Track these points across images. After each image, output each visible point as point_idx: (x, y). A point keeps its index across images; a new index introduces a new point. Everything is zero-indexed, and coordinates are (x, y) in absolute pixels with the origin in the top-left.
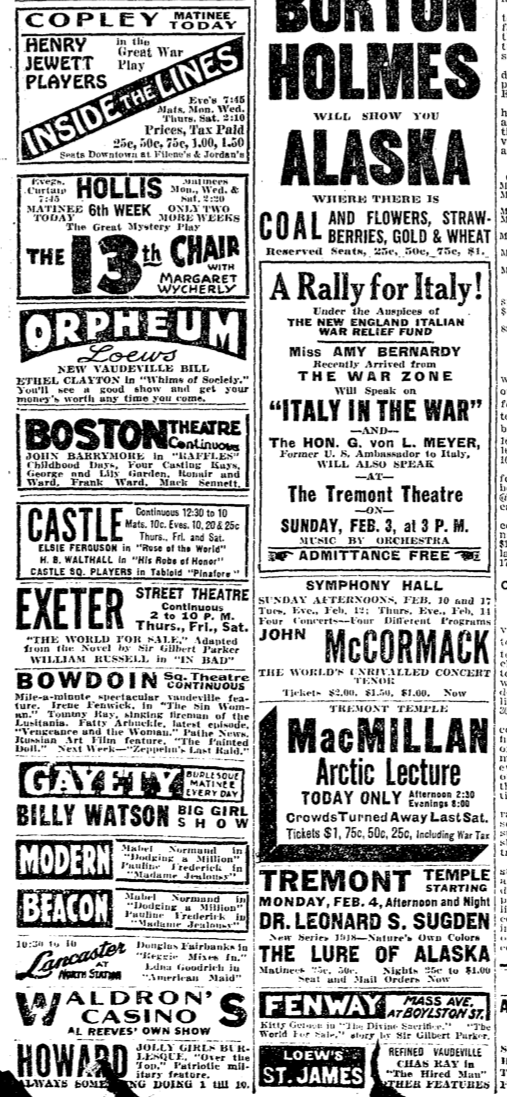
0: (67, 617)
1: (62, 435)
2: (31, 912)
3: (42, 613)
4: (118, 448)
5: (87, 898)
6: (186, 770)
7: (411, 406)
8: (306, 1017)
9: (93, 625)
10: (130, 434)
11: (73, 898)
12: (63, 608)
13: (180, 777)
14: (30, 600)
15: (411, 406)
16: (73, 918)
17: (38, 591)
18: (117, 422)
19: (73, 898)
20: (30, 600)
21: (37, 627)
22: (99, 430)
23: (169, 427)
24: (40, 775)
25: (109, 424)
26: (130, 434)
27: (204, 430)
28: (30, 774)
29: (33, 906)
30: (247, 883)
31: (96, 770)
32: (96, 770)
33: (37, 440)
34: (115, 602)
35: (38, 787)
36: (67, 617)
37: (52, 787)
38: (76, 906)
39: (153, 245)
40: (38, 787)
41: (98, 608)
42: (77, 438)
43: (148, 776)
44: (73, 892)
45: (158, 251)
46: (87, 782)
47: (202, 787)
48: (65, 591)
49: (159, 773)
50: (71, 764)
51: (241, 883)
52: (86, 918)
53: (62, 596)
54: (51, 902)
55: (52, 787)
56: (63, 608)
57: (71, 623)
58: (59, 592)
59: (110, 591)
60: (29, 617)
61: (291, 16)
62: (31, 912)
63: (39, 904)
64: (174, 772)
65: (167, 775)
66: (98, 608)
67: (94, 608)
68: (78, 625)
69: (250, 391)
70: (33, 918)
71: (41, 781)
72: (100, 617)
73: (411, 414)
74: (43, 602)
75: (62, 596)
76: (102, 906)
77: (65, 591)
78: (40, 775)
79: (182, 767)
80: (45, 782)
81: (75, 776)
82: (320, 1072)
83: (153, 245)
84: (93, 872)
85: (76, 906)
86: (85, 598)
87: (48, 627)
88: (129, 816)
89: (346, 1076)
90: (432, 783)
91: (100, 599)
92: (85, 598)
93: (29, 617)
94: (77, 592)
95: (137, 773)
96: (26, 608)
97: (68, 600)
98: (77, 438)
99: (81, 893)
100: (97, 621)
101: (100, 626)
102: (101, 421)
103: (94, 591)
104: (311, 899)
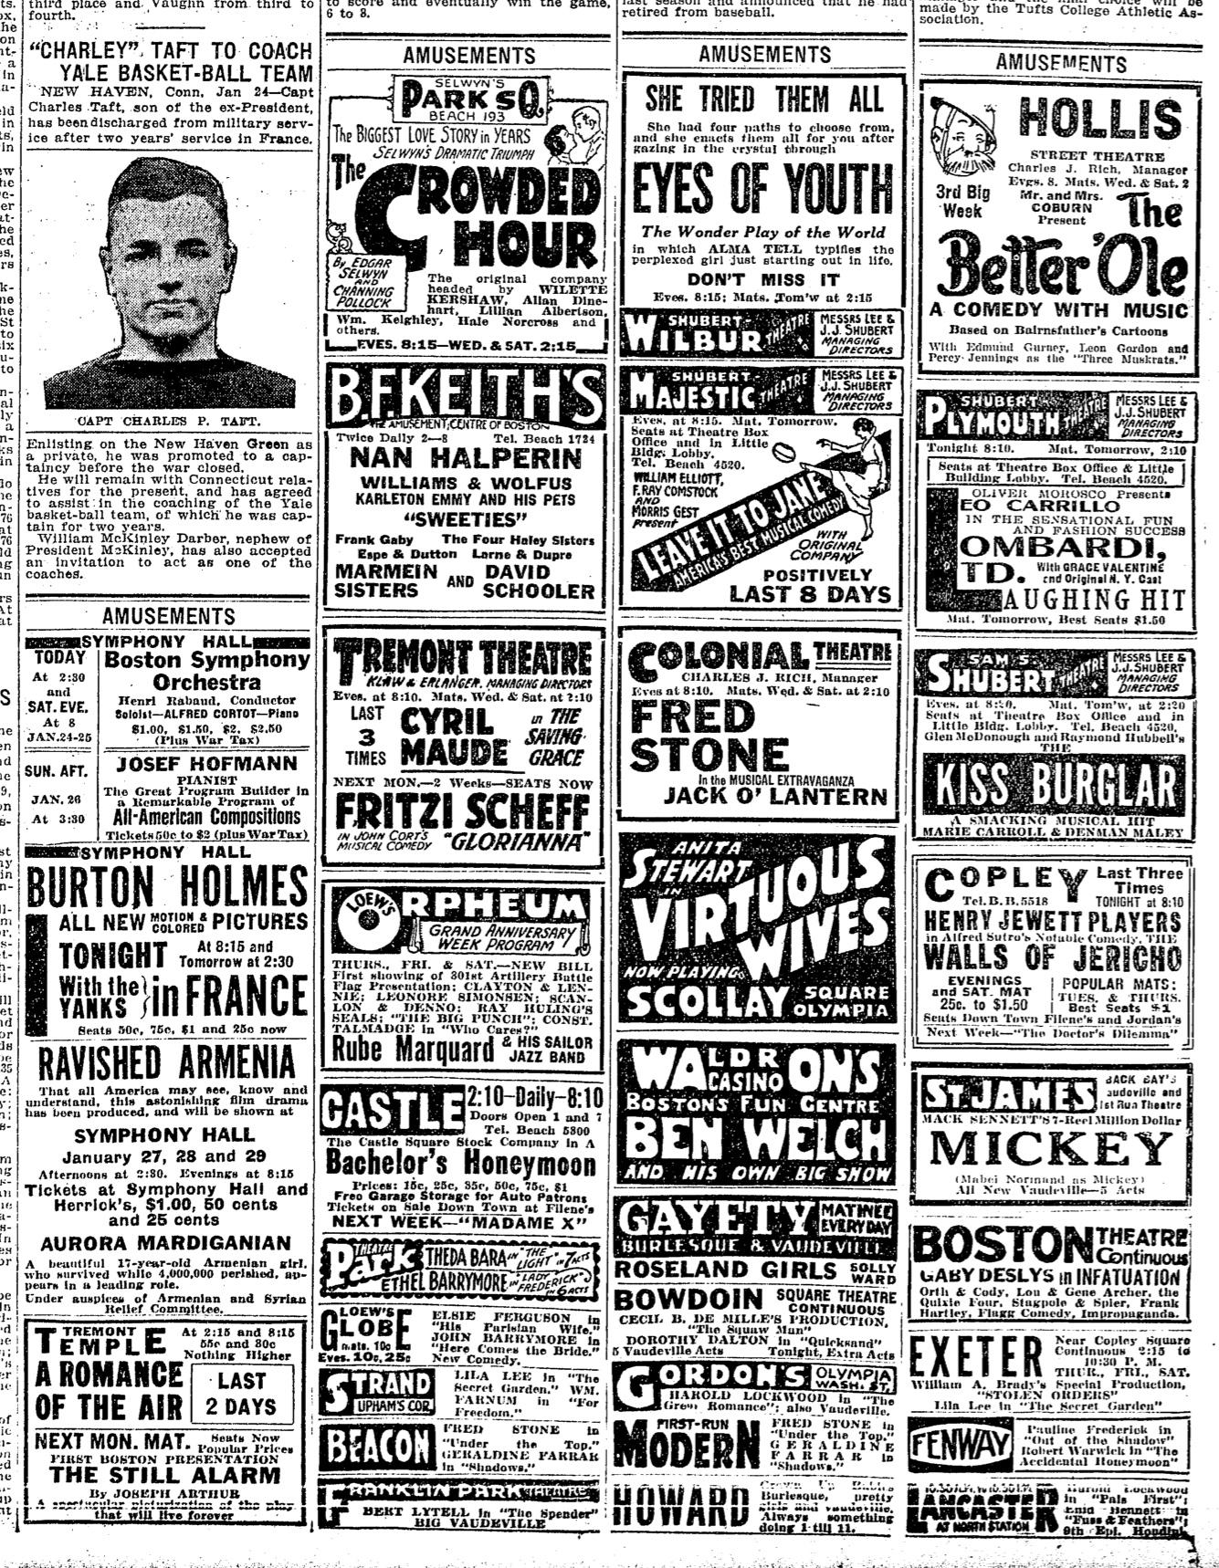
0: (973, 1364)
1: (958, 1244)
2: (337, 1452)
3: (940, 1361)
4: (1031, 1260)
5: (403, 1435)
8: (555, 367)
10: (1047, 1244)
11: (388, 1434)
13: (814, 1211)
16: (388, 1458)
18: (1028, 1229)
19: (388, 1434)
20: (926, 1349)
22: (1007, 1240)
23: (1097, 1235)
24: (636, 1211)
25: (1019, 1232)
26: (1047, 1244)
27: (1143, 1239)
29: (339, 1444)
30: (602, 867)
31: (706, 1204)
33: (927, 1250)
35: (634, 1226)
36: (973, 1364)
38: (391, 1443)
40: (634, 1226)
42: (976, 1247)
44: (388, 1426)
46: (697, 1218)
49: (791, 1207)
52: (404, 1458)
54: (362, 1439)
62: (337, 1452)
63: (347, 1443)
64: (808, 1205)
65: (800, 1210)
67: (1007, 1356)
70: (340, 1459)
76: (422, 1444)
81: (680, 1211)
82: (795, 492)
85: (391, 1443)
89: (801, 1138)
91: (1017, 1348)
94: (986, 1340)
95: (763, 1207)
97: (974, 1348)
98: (976, 1247)
99: (397, 1428)
102: (1009, 1229)
104: (244, 1402)
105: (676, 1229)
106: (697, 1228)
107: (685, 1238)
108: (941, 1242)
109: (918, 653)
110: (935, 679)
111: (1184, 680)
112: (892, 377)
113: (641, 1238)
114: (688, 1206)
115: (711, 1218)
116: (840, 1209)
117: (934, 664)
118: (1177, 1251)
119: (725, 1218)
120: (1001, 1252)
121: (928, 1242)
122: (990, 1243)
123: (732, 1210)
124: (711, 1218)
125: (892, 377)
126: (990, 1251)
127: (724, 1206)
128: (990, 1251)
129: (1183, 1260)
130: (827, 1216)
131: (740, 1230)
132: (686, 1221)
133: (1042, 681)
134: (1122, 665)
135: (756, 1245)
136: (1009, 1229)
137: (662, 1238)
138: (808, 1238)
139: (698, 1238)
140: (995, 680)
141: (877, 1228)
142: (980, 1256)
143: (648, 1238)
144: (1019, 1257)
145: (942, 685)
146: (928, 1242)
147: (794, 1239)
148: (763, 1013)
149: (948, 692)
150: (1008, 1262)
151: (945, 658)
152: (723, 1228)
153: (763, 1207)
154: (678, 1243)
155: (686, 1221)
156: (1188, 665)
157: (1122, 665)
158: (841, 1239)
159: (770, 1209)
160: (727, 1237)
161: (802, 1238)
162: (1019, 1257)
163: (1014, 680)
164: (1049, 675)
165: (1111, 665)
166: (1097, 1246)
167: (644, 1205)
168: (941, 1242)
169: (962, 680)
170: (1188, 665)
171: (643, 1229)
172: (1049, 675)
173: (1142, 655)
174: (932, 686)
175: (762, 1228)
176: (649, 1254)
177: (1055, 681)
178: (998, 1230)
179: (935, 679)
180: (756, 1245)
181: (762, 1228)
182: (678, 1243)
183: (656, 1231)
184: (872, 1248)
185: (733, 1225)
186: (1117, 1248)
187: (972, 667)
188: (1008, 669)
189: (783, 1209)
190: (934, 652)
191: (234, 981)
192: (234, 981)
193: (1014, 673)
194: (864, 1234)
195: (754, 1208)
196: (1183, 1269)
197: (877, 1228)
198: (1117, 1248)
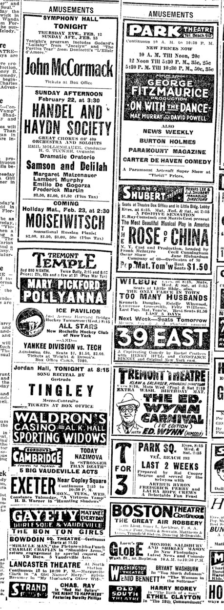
0: (32, 489)
1: (128, 511)
3: (22, 487)
4: (151, 516)
6: (81, 510)
7: (140, 546)
9: (43, 492)
10: (157, 511)
12: (31, 485)
13: (78, 513)
14: (17, 482)
15: (140, 546)
17: (20, 478)
20: (17, 482)
21: (20, 492)
22: (144, 510)
23: (174, 509)
24: (19, 514)
26: (157, 511)
27: (189, 510)
28: (15, 513)
31: (41, 511)
32: (41, 511)
33: (117, 512)
34: (52, 484)
35: (18, 519)
37: (23, 519)
39: (104, 163)
40: (18, 519)
41: (45, 485)
42: (134, 512)
43: (65, 513)
45: (106, 166)
46: (38, 516)
47: (87, 515)
48: (31, 478)
49: (70, 512)
50: (30, 509)
51: (210, 182)
53: (30, 480)
55: (23, 519)
56: (31, 485)
57: (34, 492)
58: (29, 478)
59: (50, 479)
60: (16, 489)
61: (179, 198)
64: (76, 511)
65: (73, 513)
66: (45, 485)
67: (43, 486)
68: (37, 492)
69: (220, 7)
71: (18, 516)
72: (46, 489)
73: (140, 552)
74: (22, 483)
75: (30, 480)
77: (31, 478)
78: (19, 514)
79: (79, 509)
80: (20, 517)
81: (33, 514)
83: (104, 163)
84: (42, 462)
86: (40, 481)
87: (24, 493)
88: (84, 223)
90: (200, 300)
91: (46, 482)
92: (40, 481)
93: (16, 489)
94: (37, 479)
95: (60, 512)
96: (15, 485)
98: (134, 512)
100: (65, 115)
101: (46, 493)
103: (43, 479)
105: (32, 519)
106: (38, 519)
107: (35, 523)
108: (122, 510)
109: (120, 186)
110: (125, 195)
111: (209, 196)
112: (209, 190)
113: (20, 522)
114: (35, 512)
115: (43, 516)
116: (87, 513)
117: (125, 190)
118: (200, 514)
119: (48, 516)
120: (141, 514)
121: (117, 510)
122: (139, 511)
123: (50, 513)
124: (43, 516)
125: (209, 190)
126: (138, 513)
127: (47, 512)
128: (138, 513)
129: (202, 517)
130: (83, 515)
131: (53, 520)
132: (35, 517)
133: (161, 196)
134: (189, 192)
135: (58, 524)
136: (145, 506)
137: (27, 522)
138: (77, 522)
139: (39, 523)
140: (145, 196)
141: (99, 519)
142: (135, 515)
143: (22, 522)
144: (148, 515)
145: (128, 196)
146: (117, 510)
147: (71, 522)
148: (74, 301)
149: (130, 199)
150: (144, 517)
151: (129, 188)
152: (47, 519)
153: (60, 512)
154: (32, 524)
155: (35, 517)
156: (211, 192)
157: (189, 192)
158: (88, 523)
159: (63, 513)
160: (48, 522)
161: (74, 522)
162: (148, 515)
163: (152, 196)
164: (163, 194)
165: (185, 191)
166: (174, 512)
167: (21, 512)
168: (122, 510)
169: (134, 195)
170: (211, 192)
171: (20, 520)
172: (163, 194)
173: (196, 188)
174: (125, 197)
175: (60, 519)
176: (22, 527)
177: (165, 197)
178: (141, 507)
179: (125, 195)
180: (58, 524)
181: (60, 519)
182: (32, 524)
183: (25, 520)
184: (97, 525)
185: (50, 518)
186: (180, 513)
187: (137, 191)
188: (149, 192)
189: (68, 513)
190: (125, 186)
191: (43, 106)
192: (43, 106)
193: (152, 193)
194: (95, 521)
195: (58, 512)
196: (203, 520)
197: (99, 519)
198: (180, 513)
